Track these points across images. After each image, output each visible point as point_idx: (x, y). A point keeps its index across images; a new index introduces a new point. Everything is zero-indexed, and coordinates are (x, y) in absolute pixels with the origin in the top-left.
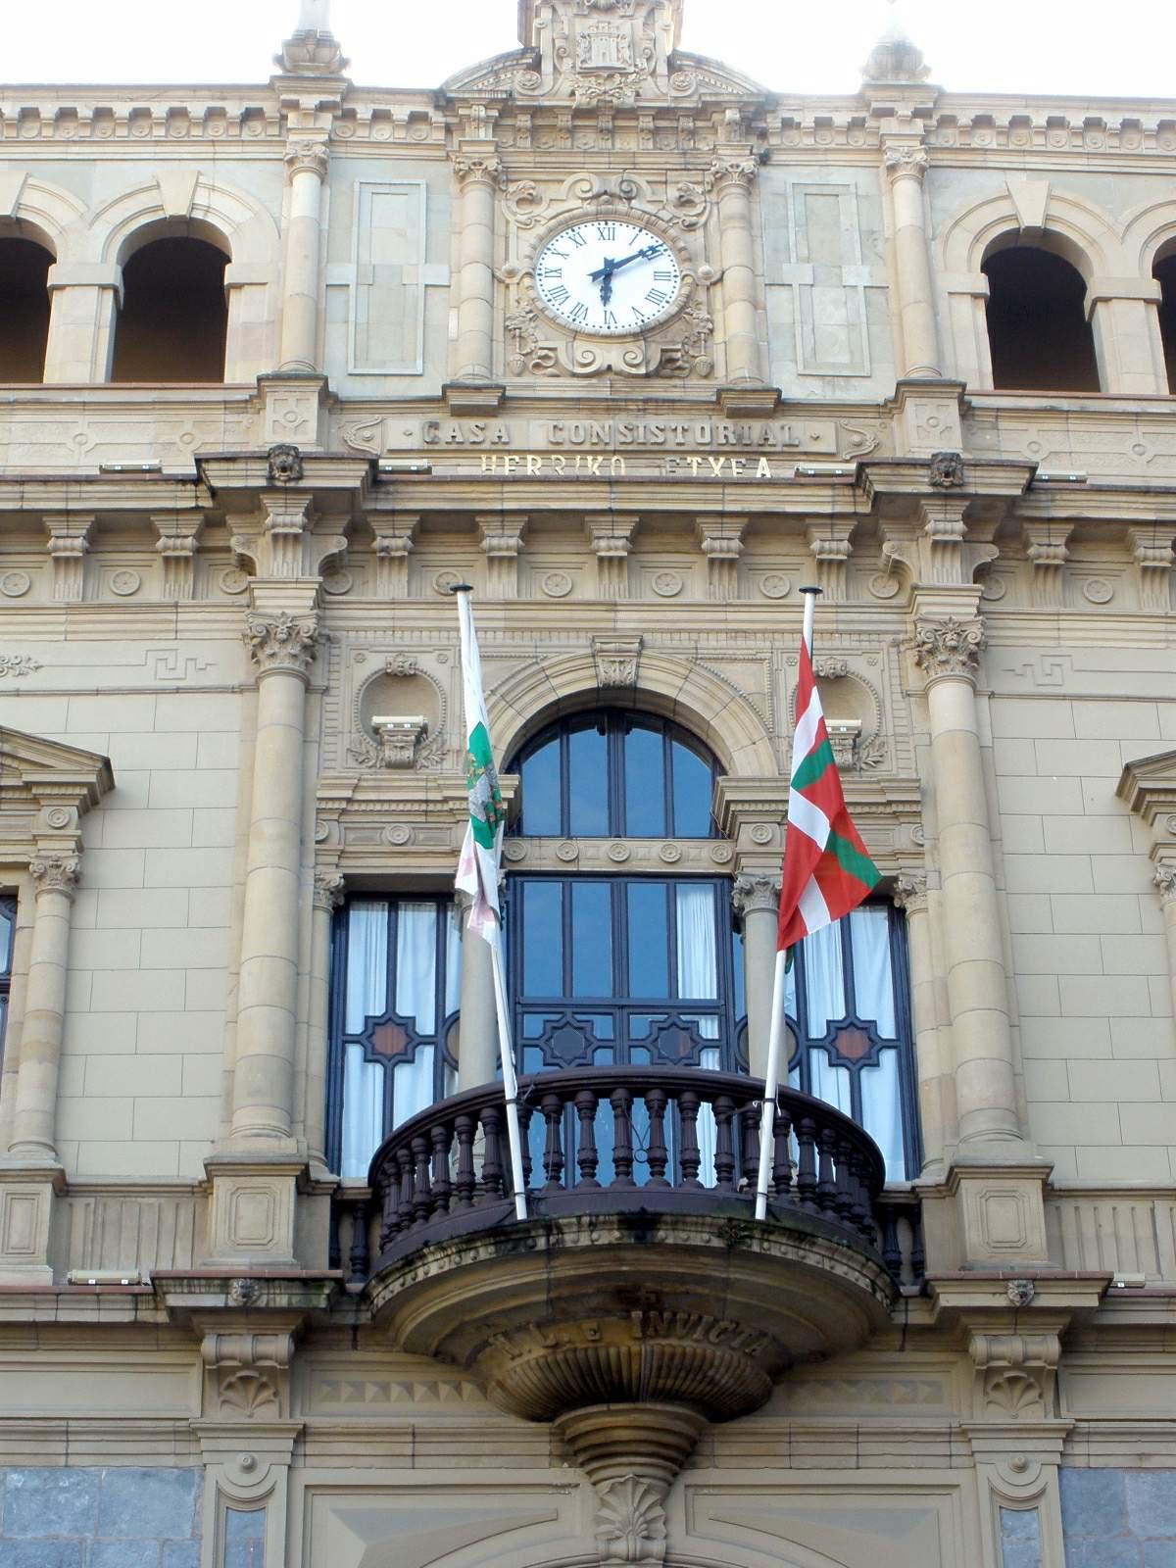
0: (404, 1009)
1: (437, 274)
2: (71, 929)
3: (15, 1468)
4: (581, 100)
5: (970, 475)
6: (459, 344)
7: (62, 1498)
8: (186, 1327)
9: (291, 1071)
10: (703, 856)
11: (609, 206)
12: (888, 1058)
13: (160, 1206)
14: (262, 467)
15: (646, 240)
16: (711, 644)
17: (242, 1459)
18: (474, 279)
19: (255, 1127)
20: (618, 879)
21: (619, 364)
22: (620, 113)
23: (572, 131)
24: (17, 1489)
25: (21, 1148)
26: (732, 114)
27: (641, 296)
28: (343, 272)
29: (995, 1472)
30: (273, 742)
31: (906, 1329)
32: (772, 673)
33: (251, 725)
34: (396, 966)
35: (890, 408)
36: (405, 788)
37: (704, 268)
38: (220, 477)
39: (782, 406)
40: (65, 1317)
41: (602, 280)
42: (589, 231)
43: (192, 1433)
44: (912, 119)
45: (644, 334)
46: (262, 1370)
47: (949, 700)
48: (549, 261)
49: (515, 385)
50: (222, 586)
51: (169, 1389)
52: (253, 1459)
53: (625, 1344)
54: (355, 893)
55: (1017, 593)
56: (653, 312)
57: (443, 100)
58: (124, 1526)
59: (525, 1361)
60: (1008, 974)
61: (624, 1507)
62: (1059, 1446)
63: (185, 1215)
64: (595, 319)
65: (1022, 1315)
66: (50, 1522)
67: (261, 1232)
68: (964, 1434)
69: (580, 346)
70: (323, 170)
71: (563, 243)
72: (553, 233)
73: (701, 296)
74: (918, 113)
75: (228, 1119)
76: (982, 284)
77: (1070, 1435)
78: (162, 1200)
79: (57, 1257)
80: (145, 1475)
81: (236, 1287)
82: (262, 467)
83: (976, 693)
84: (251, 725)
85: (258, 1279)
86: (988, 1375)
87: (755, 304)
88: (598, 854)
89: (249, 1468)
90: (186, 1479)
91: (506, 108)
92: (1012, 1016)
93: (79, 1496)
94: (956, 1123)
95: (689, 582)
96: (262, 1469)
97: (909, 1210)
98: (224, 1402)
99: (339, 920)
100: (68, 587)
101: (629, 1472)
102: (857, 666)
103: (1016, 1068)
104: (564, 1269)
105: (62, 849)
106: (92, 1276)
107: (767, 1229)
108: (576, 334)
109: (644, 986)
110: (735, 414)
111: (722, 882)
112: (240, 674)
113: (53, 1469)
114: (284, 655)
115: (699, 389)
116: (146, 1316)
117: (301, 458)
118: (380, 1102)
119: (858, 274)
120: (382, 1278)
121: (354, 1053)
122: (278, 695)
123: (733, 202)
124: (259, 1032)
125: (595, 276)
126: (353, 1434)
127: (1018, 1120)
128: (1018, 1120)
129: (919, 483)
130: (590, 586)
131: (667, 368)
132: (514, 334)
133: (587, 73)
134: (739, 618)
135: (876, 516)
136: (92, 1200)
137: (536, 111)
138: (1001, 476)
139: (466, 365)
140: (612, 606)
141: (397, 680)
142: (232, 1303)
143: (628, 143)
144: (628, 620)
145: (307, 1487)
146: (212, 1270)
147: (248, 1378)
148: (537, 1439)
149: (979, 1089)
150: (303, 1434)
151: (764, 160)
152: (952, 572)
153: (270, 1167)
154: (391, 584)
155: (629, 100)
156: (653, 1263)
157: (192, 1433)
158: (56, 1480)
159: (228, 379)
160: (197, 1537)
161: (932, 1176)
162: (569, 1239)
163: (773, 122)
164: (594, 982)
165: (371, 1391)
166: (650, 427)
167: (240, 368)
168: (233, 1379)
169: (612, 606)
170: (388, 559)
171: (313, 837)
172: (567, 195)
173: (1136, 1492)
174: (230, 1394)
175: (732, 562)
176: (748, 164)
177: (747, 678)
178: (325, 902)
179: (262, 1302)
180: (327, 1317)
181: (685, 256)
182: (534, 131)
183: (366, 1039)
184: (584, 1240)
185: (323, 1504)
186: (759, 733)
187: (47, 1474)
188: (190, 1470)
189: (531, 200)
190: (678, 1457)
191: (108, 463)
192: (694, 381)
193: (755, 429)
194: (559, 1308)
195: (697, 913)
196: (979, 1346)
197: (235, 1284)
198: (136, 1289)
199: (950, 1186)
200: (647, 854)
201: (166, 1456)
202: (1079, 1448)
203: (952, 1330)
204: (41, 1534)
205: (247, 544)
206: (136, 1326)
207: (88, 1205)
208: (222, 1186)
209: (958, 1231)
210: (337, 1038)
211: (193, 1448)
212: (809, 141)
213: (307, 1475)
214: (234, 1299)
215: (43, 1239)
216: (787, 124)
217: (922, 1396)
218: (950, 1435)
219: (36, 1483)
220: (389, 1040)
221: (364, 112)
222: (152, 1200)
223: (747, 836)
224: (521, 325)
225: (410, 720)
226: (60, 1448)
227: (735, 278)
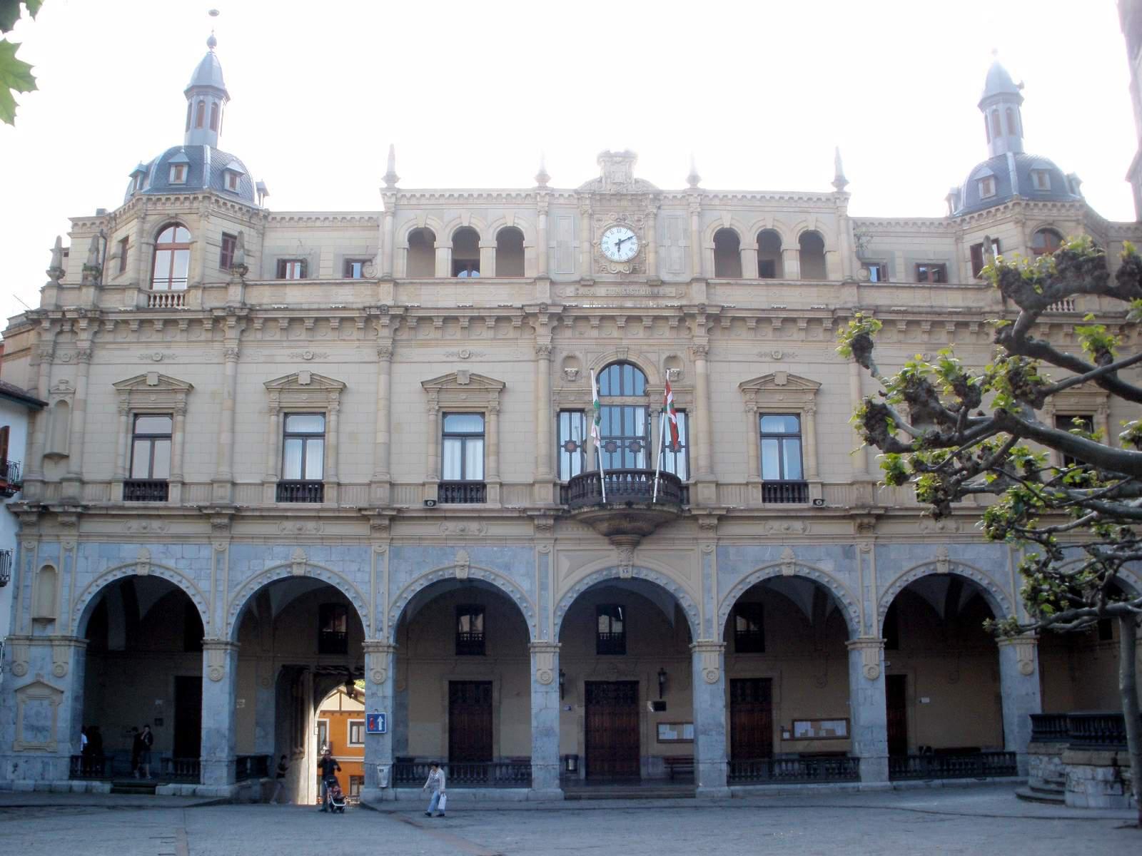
0: (574, 439)
1: (576, 243)
2: (498, 422)
4: (612, 192)
5: (707, 308)
6: (582, 267)
8: (531, 518)
9: (550, 456)
10: (643, 401)
11: (621, 222)
12: (683, 450)
14: (538, 308)
15: (630, 234)
16: (645, 348)
18: (586, 245)
19: (543, 472)
20: (622, 407)
21: (622, 270)
22: (622, 195)
23: (609, 200)
26: (651, 196)
27: (628, 251)
28: (553, 244)
29: (702, 547)
30: (543, 377)
31: (685, 517)
32: (659, 356)
33: (537, 372)
34: (570, 427)
35: (689, 284)
36: (573, 387)
37: (644, 242)
38: (528, 310)
39: (663, 283)
41: (618, 244)
42: (615, 230)
43: (532, 539)
44: (698, 199)
45: (629, 261)
47: (700, 365)
48: (605, 239)
49: (596, 277)
50: (527, 334)
51: (526, 530)
53: (626, 525)
54: (563, 410)
55: (718, 334)
56: (631, 254)
57: (576, 192)
59: (604, 526)
60: (710, 433)
61: (623, 555)
64: (616, 257)
65: (709, 515)
67: (546, 497)
68: (696, 539)
69: (613, 265)
70: (547, 214)
71: (608, 233)
72: (606, 231)
73: (643, 250)
74: (699, 195)
76: (713, 245)
77: (719, 539)
79: (501, 501)
81: (542, 511)
82: (538, 308)
83: (707, 361)
84: (537, 372)
86: (702, 527)
87: (656, 252)
88: (618, 400)
91: (593, 194)
92: (711, 443)
94: (698, 469)
95: (638, 332)
97: (687, 487)
99: (558, 416)
100: (491, 334)
101: (625, 548)
102: (679, 354)
103: (711, 455)
104: (613, 512)
105: (495, 404)
106: (510, 506)
107: (656, 504)
108: (612, 261)
109: (628, 433)
110: (650, 286)
111: (647, 407)
112: (533, 358)
114: (544, 355)
115: (642, 278)
116: (522, 515)
117: (547, 305)
118: (571, 467)
119: (682, 243)
120: (574, 509)
121: (563, 449)
122: (543, 364)
123: (651, 223)
124: (543, 450)
125: (616, 244)
126: (566, 539)
127: (711, 469)
128: (711, 469)
129: (695, 311)
130: (616, 333)
131: (634, 271)
132: (596, 261)
133: (614, 183)
134: (651, 341)
135: (684, 317)
137: (601, 195)
138: (715, 309)
139: (586, 275)
140: (621, 339)
141: (570, 358)
143: (624, 203)
144: (625, 342)
146: (537, 506)
148: (606, 540)
149: (703, 462)
150: (556, 540)
151: (659, 208)
152: (702, 331)
154: (568, 333)
155: (625, 192)
156: (631, 511)
157: (532, 539)
159: (526, 276)
160: (534, 561)
161: (692, 481)
162: (615, 507)
163: (662, 197)
164: (616, 432)
165: (570, 529)
166: (631, 289)
167: (530, 272)
169: (621, 339)
170: (567, 327)
171: (553, 399)
172: (609, 219)
173: (732, 551)
175: (649, 327)
176: (655, 211)
177: (653, 357)
178: (555, 414)
180: (560, 517)
181: (639, 238)
182: (600, 200)
183: (565, 446)
184: (618, 507)
185: (561, 554)
186: (656, 372)
189: (599, 220)
190: (635, 544)
191: (499, 304)
192: (641, 275)
193: (656, 290)
194: (611, 518)
195: (640, 413)
196: (700, 522)
199: (696, 484)
200: (629, 400)
202: (721, 542)
203: (695, 518)
205: (534, 323)
209: (697, 494)
210: (559, 446)
212: (671, 203)
214: (542, 512)
215: (498, 498)
216: (665, 197)
217: (686, 532)
218: (694, 539)
220: (571, 446)
221: (557, 195)
223: (653, 398)
224: (599, 259)
225: (574, 370)
227: (651, 245)
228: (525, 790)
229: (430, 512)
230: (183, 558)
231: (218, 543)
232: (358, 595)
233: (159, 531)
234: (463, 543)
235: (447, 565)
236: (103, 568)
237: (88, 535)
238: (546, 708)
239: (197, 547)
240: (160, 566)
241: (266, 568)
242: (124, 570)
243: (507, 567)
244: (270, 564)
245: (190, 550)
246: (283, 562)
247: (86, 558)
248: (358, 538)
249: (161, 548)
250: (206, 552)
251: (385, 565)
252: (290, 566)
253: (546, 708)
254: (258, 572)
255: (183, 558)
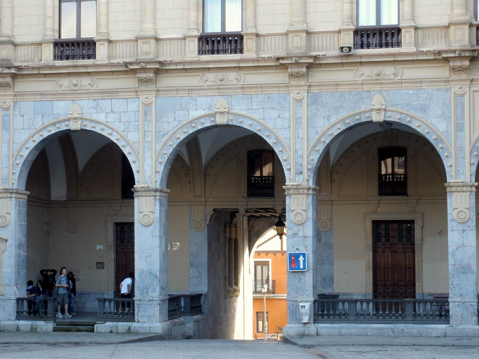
3: (411, 89)
7: (421, 95)
8: (446, 60)
13: (438, 31)
17: (459, 86)
24: (411, 94)
25: (406, 20)
40: (419, 58)
46: (463, 68)
51: (440, 72)
52: (462, 86)
58: (434, 101)
62: (155, 93)
63: (443, 33)
66: (419, 100)
75: (452, 10)
78: (438, 29)
79: (416, 45)
80: (438, 90)
81: (457, 52)
85: (462, 51)
89: (461, 88)
90: (447, 90)
93: (424, 95)
96: (464, 88)
98: (454, 74)
106: (425, 49)
113: (419, 89)
136: (422, 30)
142: (456, 56)
145: (473, 91)
147: (461, 70)
150: (472, 80)
153: (464, 23)
158: (420, 92)
168: (456, 70)
174: (456, 73)
179: (463, 55)
187: (417, 90)
188: (448, 88)
197: (457, 52)
198: (435, 52)
201: (443, 86)
204: (417, 103)
206: (435, 59)
207: (422, 31)
208: (452, 28)
211: (448, 84)
213: (473, 89)
214: (457, 54)
215: (413, 41)
219: (415, 92)
222: (436, 30)
226: (420, 85)
228: (444, 326)
229: (346, 60)
230: (112, 112)
231: (144, 97)
232: (278, 141)
233: (89, 87)
234: (378, 88)
235: (363, 109)
236: (39, 124)
237: (23, 94)
238: (463, 245)
239: (125, 101)
240: (92, 121)
241: (191, 118)
242: (58, 126)
243: (423, 109)
244: (194, 114)
245: (118, 105)
246: (207, 112)
247: (23, 116)
248: (278, 86)
249: (92, 103)
250: (133, 105)
251: (303, 112)
252: (214, 115)
253: (463, 245)
254: (185, 122)
255: (112, 112)
